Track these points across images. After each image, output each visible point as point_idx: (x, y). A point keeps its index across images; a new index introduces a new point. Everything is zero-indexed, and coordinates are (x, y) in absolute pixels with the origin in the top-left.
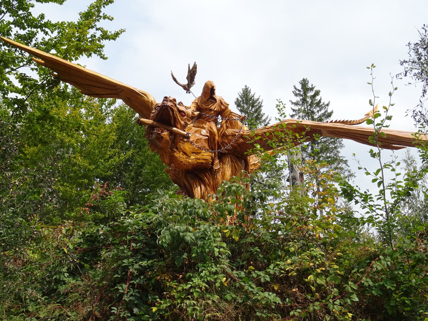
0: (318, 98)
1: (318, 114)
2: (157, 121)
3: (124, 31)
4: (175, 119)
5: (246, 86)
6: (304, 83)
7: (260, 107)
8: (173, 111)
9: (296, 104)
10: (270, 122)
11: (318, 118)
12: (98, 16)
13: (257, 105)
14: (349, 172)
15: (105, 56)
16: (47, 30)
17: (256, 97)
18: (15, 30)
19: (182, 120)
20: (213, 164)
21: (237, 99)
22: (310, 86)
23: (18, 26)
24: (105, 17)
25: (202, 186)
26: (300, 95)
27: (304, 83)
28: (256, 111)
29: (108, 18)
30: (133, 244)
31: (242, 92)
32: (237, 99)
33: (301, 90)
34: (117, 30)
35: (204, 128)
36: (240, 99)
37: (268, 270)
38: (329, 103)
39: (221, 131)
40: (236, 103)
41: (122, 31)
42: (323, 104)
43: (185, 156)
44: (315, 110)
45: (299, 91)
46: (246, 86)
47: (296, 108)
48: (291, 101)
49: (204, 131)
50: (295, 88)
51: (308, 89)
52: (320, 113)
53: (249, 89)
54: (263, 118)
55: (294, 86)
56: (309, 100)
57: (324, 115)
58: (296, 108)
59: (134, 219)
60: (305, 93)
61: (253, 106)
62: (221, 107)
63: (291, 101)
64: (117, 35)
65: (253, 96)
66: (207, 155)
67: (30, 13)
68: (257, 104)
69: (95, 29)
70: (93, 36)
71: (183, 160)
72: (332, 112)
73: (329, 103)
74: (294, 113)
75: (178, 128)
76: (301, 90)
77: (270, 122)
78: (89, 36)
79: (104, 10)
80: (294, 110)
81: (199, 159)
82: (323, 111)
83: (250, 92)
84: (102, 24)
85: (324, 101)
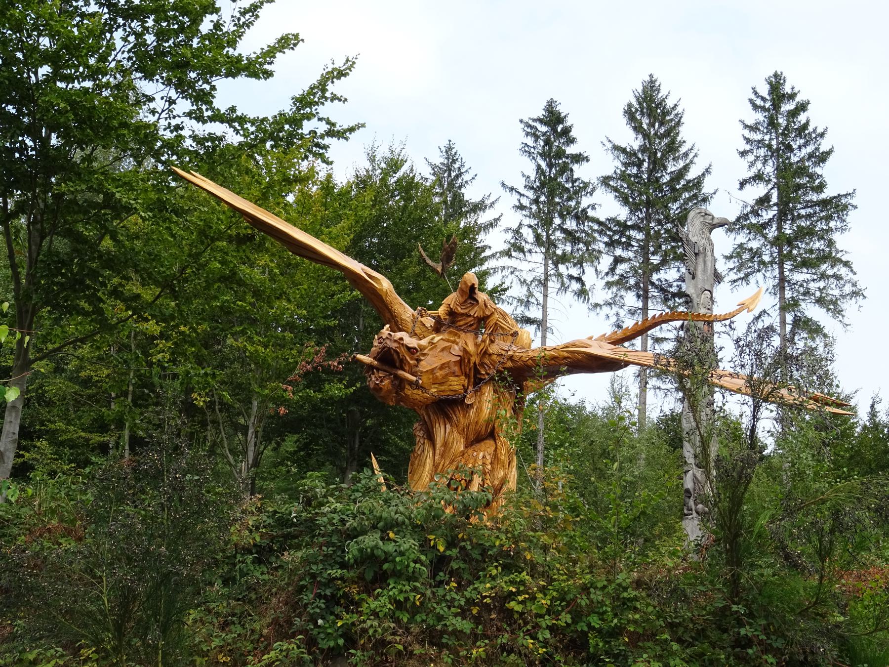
0: (802, 118)
1: (798, 154)
2: (378, 360)
5: (651, 76)
7: (678, 124)
9: (754, 128)
10: (696, 160)
11: (798, 162)
12: (323, 97)
13: (671, 120)
14: (854, 285)
15: (330, 160)
17: (670, 103)
18: (191, 127)
19: (412, 359)
20: (465, 397)
22: (787, 89)
24: (334, 98)
25: (448, 426)
26: (763, 109)
28: (667, 134)
29: (340, 100)
31: (640, 89)
32: (630, 105)
33: (768, 98)
34: (352, 124)
35: (457, 344)
37: (465, 593)
38: (826, 130)
39: (481, 347)
40: (626, 112)
42: (815, 130)
45: (764, 99)
46: (651, 76)
49: (456, 347)
50: (756, 93)
51: (784, 95)
53: (657, 84)
54: (683, 150)
55: (753, 89)
56: (782, 121)
57: (810, 156)
58: (757, 136)
60: (776, 106)
61: (662, 124)
62: (484, 312)
65: (663, 100)
67: (214, 86)
68: (672, 116)
69: (316, 118)
70: (313, 133)
71: (418, 397)
72: (831, 151)
73: (826, 130)
74: (748, 147)
75: (405, 371)
76: (768, 98)
77: (696, 160)
79: (332, 88)
80: (748, 141)
81: (443, 391)
82: (810, 149)
84: (326, 110)
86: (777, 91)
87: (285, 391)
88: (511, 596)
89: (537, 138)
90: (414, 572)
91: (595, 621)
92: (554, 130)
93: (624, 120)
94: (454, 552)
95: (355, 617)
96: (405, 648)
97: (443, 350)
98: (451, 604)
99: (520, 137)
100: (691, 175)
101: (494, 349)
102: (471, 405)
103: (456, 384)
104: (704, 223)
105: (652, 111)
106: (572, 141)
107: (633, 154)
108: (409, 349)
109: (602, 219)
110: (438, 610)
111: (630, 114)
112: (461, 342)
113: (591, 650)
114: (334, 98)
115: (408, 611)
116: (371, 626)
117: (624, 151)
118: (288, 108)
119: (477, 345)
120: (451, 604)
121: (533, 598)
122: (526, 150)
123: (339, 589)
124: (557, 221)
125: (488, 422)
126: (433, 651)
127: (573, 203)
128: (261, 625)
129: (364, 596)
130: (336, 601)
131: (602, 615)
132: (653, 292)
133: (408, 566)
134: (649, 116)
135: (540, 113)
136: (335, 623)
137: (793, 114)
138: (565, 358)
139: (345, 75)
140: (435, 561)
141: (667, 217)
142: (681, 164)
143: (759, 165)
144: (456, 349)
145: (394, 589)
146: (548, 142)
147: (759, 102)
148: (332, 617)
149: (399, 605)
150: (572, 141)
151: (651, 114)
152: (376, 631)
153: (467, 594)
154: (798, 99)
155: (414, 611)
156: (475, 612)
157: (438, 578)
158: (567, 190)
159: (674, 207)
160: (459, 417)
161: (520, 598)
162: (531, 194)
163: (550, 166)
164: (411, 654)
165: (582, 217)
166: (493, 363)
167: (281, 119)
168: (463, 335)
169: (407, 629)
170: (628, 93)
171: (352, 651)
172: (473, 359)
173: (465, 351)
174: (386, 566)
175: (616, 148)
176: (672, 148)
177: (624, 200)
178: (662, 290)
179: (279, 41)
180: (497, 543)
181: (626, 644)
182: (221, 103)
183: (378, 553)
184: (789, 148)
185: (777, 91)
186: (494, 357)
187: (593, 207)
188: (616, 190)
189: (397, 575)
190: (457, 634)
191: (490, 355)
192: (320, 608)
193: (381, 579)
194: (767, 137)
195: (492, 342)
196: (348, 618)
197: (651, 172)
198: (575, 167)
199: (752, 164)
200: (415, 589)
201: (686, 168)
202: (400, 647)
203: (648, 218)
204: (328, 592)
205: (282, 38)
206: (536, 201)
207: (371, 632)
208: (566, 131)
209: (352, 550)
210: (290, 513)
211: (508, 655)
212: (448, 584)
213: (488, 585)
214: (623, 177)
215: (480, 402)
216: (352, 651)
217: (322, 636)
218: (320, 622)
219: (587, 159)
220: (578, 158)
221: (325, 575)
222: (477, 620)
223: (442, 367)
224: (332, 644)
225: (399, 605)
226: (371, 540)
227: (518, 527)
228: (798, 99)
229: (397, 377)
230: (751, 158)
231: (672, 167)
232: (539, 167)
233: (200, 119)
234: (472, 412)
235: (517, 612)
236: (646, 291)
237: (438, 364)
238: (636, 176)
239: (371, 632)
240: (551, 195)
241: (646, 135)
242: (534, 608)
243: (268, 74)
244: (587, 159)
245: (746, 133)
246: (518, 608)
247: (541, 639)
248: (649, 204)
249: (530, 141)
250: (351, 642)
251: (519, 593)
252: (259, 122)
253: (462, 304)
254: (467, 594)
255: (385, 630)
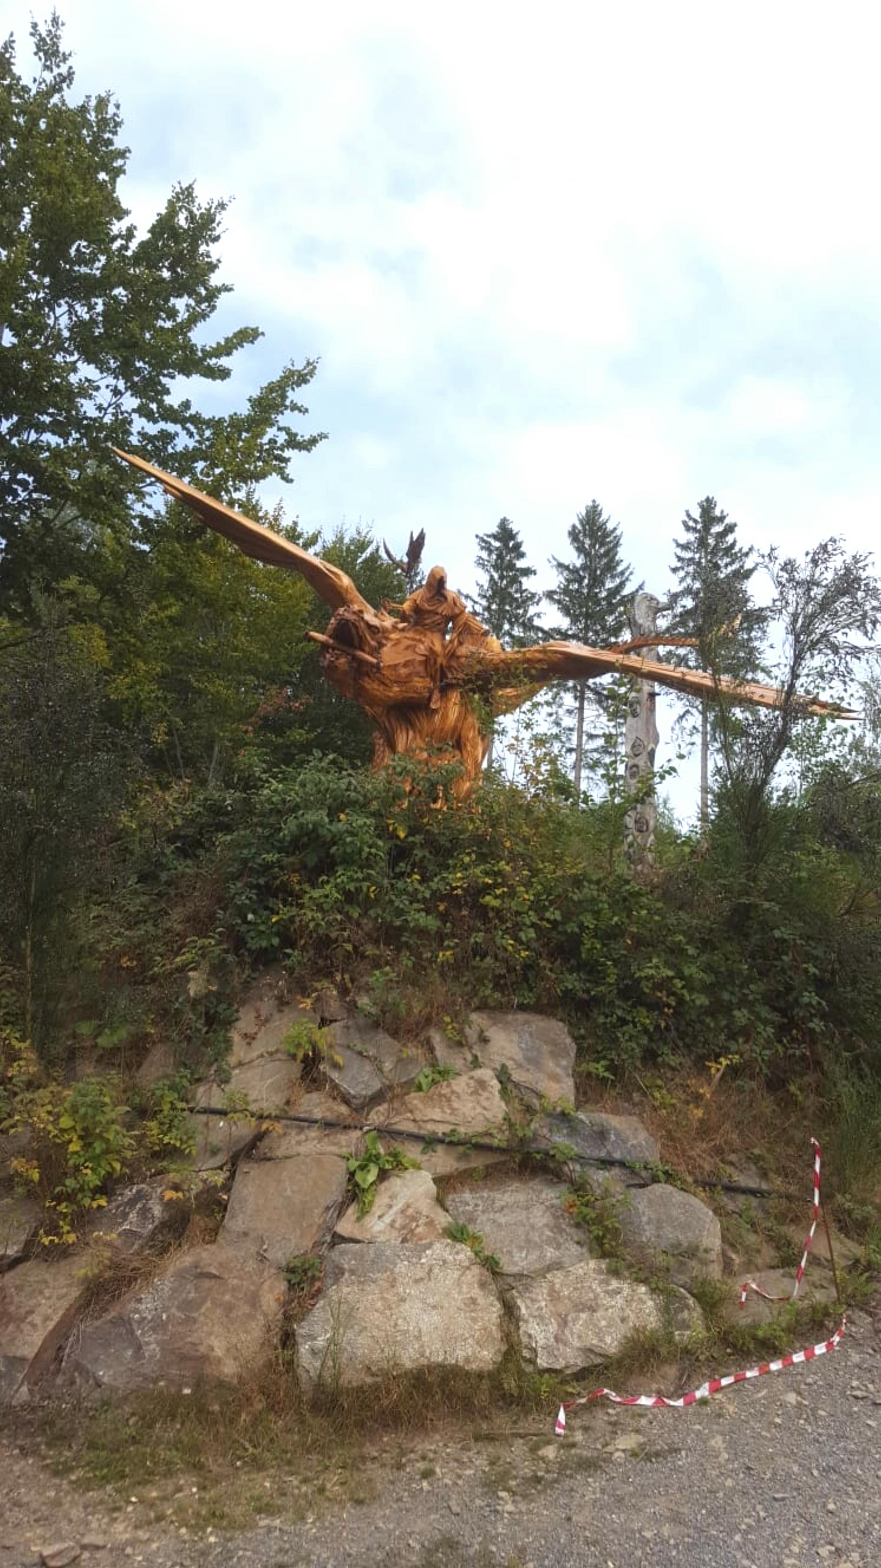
0: (730, 539)
3: (326, 437)
4: (362, 639)
6: (707, 507)
7: (617, 545)
8: (356, 627)
9: (685, 547)
16: (192, 428)
17: (610, 526)
18: (139, 424)
20: (429, 699)
21: (574, 527)
22: (717, 512)
23: (146, 416)
24: (294, 407)
25: (411, 733)
26: (695, 530)
27: (707, 507)
28: (606, 554)
30: (259, 830)
31: (584, 513)
32: (574, 527)
36: (579, 527)
40: (570, 533)
41: (323, 436)
43: (381, 688)
44: (721, 563)
45: (695, 521)
47: (688, 555)
48: (676, 541)
50: (688, 515)
52: (730, 569)
54: (620, 569)
56: (711, 541)
58: (688, 555)
59: (272, 790)
60: (707, 528)
63: (676, 541)
64: (313, 441)
66: (421, 684)
70: (273, 441)
74: (679, 565)
78: (265, 440)
80: (680, 559)
82: (736, 566)
83: (600, 514)
84: (286, 419)
85: (743, 544)
86: (708, 513)
87: (246, 732)
88: (486, 889)
89: (490, 552)
90: (367, 859)
91: (589, 921)
92: (506, 545)
93: (568, 540)
94: (418, 838)
95: (294, 911)
96: (355, 948)
97: (407, 648)
98: (414, 898)
99: (476, 551)
100: (626, 591)
101: (463, 651)
102: (435, 711)
103: (421, 684)
104: (649, 607)
105: (594, 536)
106: (522, 555)
107: (575, 571)
108: (370, 626)
109: (546, 628)
110: (396, 904)
111: (574, 535)
112: (427, 642)
113: (584, 955)
114: (294, 407)
115: (359, 905)
116: (313, 919)
117: (567, 568)
118: (244, 409)
119: (444, 647)
120: (414, 898)
121: (512, 894)
122: (480, 562)
123: (276, 878)
124: (506, 627)
125: (455, 728)
126: (389, 953)
127: (521, 611)
128: (175, 920)
129: (306, 886)
130: (272, 892)
131: (597, 914)
132: (589, 694)
133: (360, 851)
134: (591, 538)
135: (494, 529)
136: (269, 919)
137: (722, 535)
138: (540, 661)
139: (306, 381)
140: (394, 853)
141: (603, 628)
142: (618, 581)
143: (689, 580)
144: (422, 648)
145: (342, 876)
146: (500, 556)
147: (691, 524)
148: (266, 913)
149: (350, 897)
150: (522, 555)
151: (592, 535)
152: (318, 925)
153: (433, 885)
154: (727, 521)
155: (367, 905)
156: (442, 908)
157: (397, 870)
158: (516, 599)
159: (610, 620)
160: (424, 724)
161: (498, 892)
162: (484, 602)
163: (502, 578)
164: (363, 957)
165: (528, 626)
166: (461, 665)
167: (237, 424)
168: (429, 634)
169: (358, 925)
170: (572, 517)
171: (288, 951)
172: (440, 660)
173: (431, 650)
174: (333, 850)
175: (560, 565)
176: (611, 566)
177: (566, 610)
178: (597, 693)
179: (235, 335)
180: (471, 827)
181: (627, 948)
182: (173, 400)
183: (322, 831)
184: (717, 567)
185: (708, 513)
186: (463, 660)
187: (538, 615)
188: (559, 602)
189: (348, 860)
190: (421, 932)
191: (458, 657)
192: (250, 899)
193: (327, 866)
194: (697, 556)
195: (461, 644)
196: (286, 912)
197: (590, 587)
198: (524, 580)
199: (682, 580)
200: (368, 878)
201: (622, 585)
202: (349, 947)
203: (587, 628)
204: (262, 881)
205: (240, 332)
206: (488, 609)
207: (312, 925)
208: (518, 546)
209: (289, 827)
210: (225, 800)
211: (482, 960)
212: (409, 875)
213: (459, 875)
214: (566, 591)
215: (446, 708)
216: (288, 951)
217: (252, 934)
218: (250, 917)
219: (535, 572)
220: (527, 572)
221: (259, 861)
222: (444, 917)
223: (406, 665)
224: (264, 944)
225: (350, 897)
226: (315, 816)
227: (496, 808)
228: (727, 521)
229: (355, 658)
230: (682, 574)
231: (609, 584)
232: (492, 577)
233: (149, 416)
234: (437, 718)
235: (493, 908)
236: (583, 692)
237: (402, 661)
238: (577, 591)
239: (312, 925)
240: (501, 604)
241: (587, 554)
242: (514, 905)
243: (223, 374)
244: (535, 572)
245: (679, 551)
246: (496, 903)
247: (524, 939)
248: (587, 616)
249: (484, 554)
250: (289, 941)
251: (496, 886)
252: (216, 424)
253: (429, 600)
254: (433, 885)
255: (329, 924)
